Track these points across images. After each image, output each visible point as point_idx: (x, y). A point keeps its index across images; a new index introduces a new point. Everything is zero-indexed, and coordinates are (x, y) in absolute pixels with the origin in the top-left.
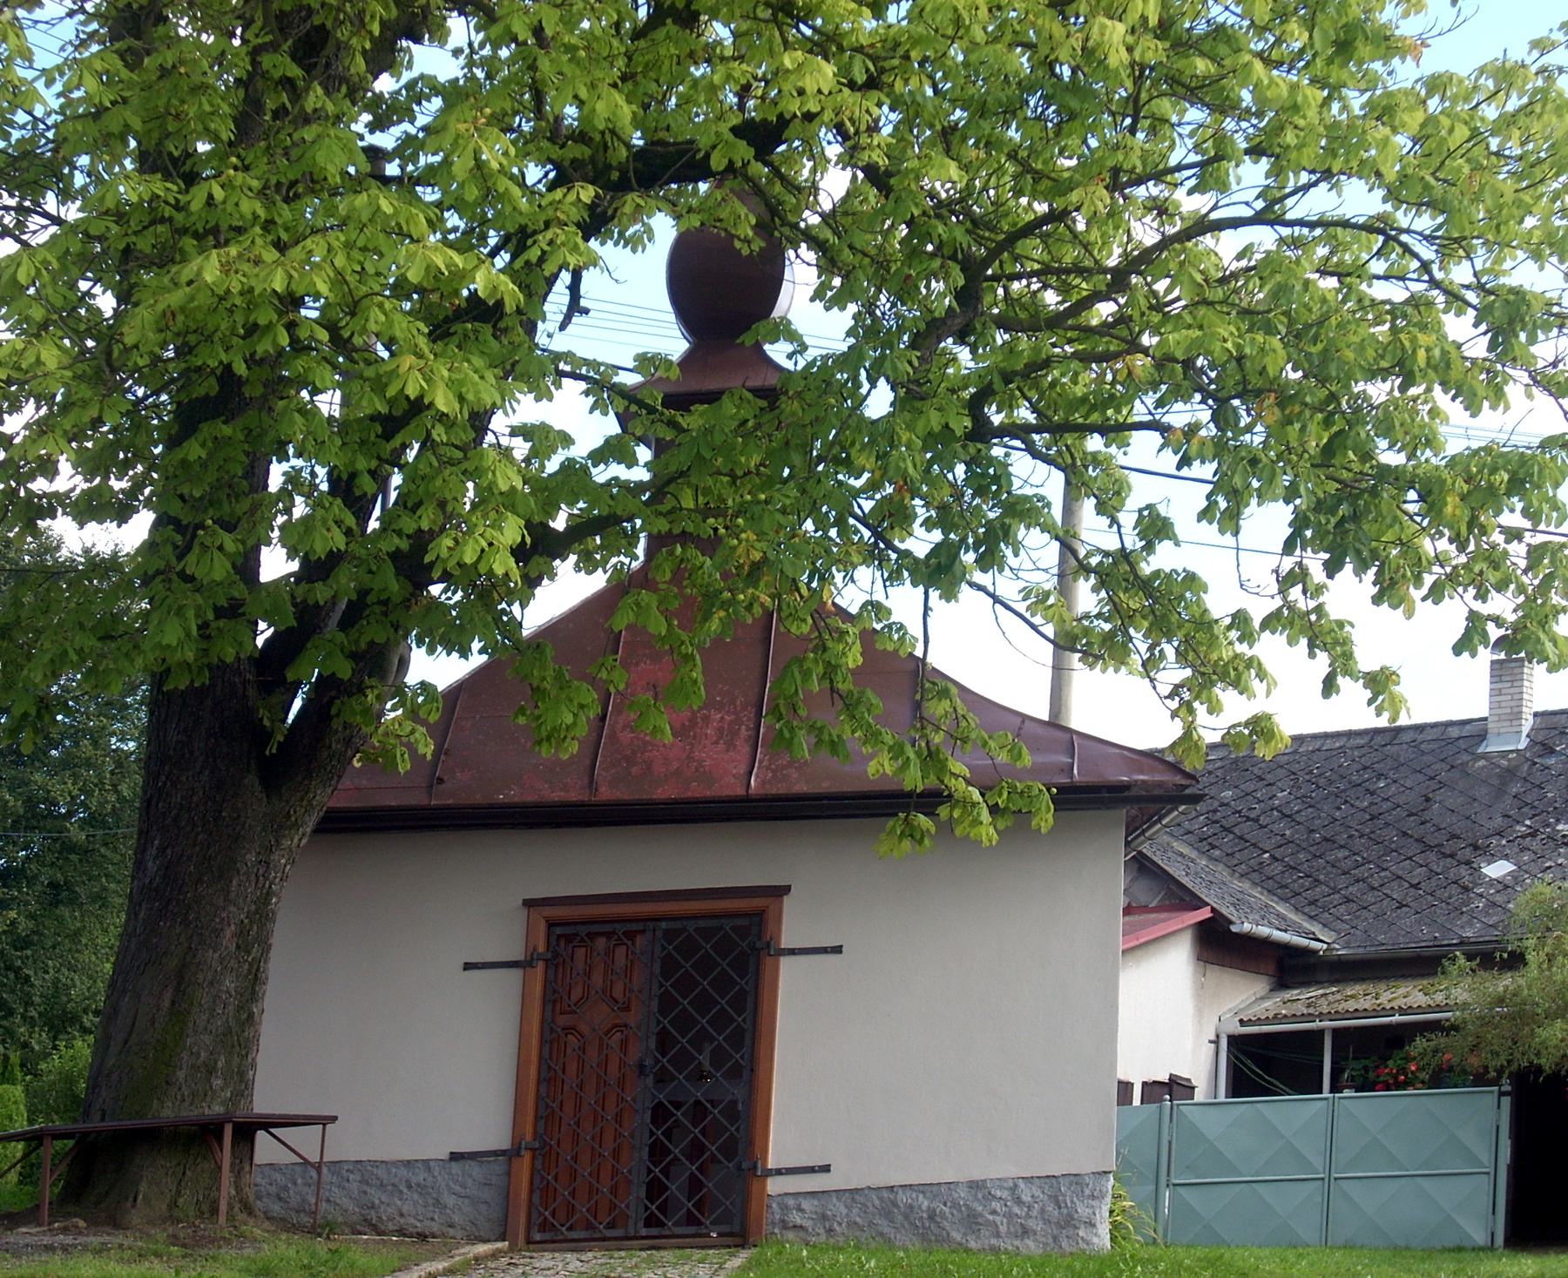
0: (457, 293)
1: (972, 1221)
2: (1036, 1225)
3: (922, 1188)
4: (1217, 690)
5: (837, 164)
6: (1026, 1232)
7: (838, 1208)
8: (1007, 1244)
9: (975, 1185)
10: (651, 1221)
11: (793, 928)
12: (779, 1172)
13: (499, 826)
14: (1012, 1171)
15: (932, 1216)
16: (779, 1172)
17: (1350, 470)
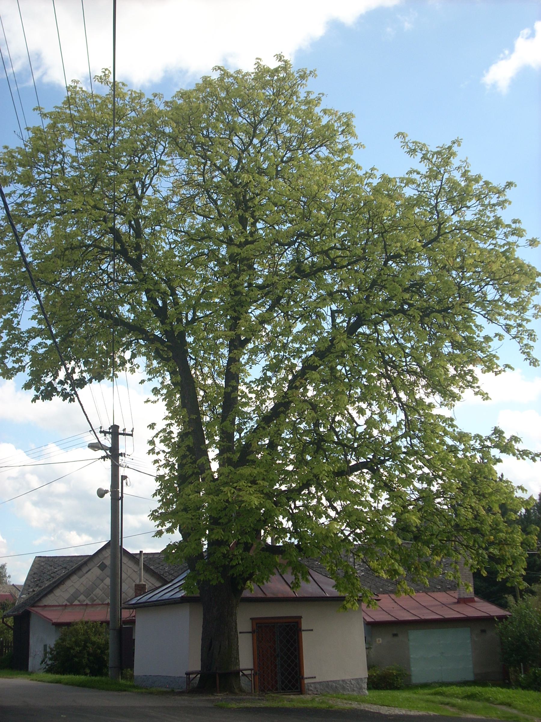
0: (273, 482)
1: (344, 688)
2: (355, 689)
3: (333, 681)
4: (177, 537)
5: (531, 585)
6: (354, 690)
7: (318, 686)
8: (351, 693)
9: (343, 681)
10: (283, 689)
11: (304, 626)
12: (309, 678)
13: (315, 597)
14: (349, 678)
15: (336, 687)
16: (309, 678)
17: (247, 363)
